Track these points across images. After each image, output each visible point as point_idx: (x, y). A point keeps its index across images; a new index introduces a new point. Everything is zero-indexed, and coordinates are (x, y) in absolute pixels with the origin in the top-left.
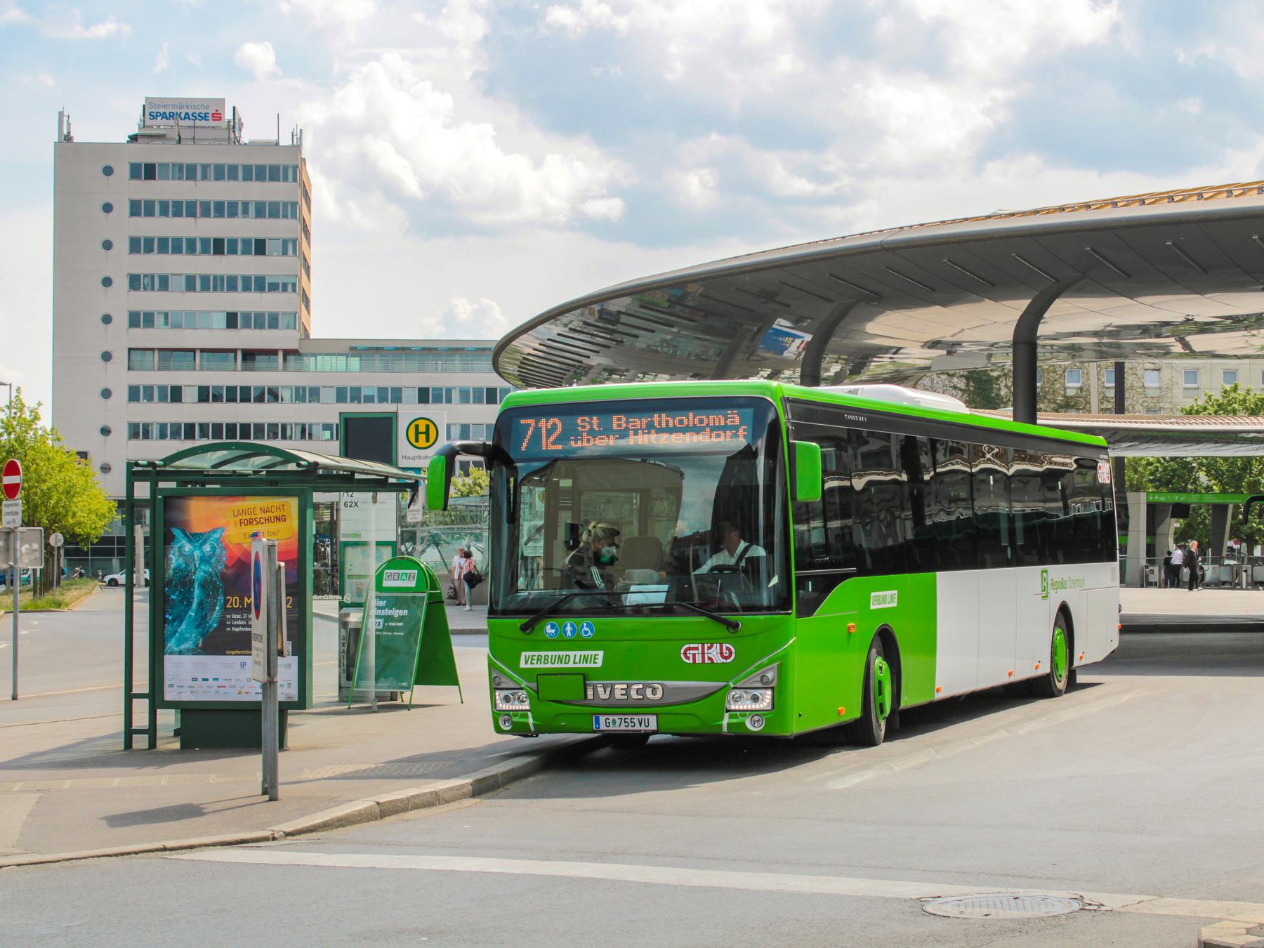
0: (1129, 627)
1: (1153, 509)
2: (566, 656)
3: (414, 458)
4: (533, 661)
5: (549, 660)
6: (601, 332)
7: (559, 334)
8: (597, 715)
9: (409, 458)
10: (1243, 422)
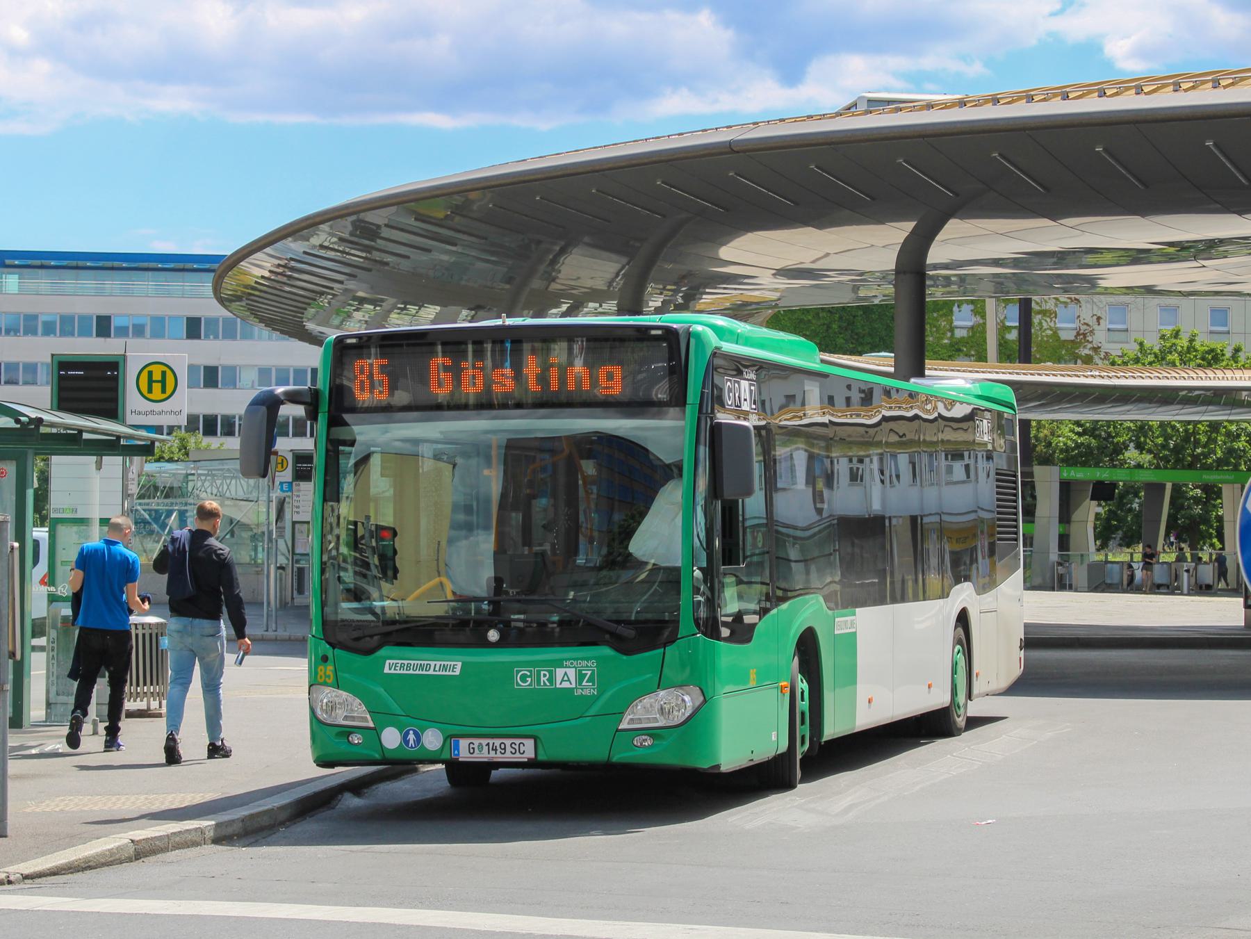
0: (1035, 640)
1: (1067, 491)
3: (146, 414)
4: (397, 668)
5: (412, 667)
6: (354, 249)
7: (305, 253)
9: (140, 413)
10: (1186, 375)
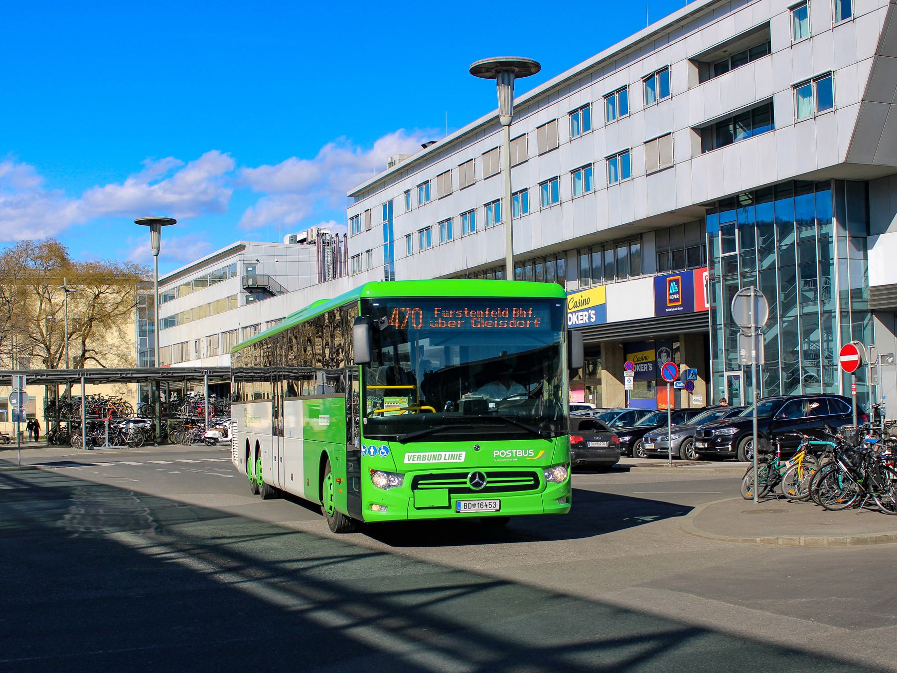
2: (439, 455)
4: (414, 459)
5: (427, 458)
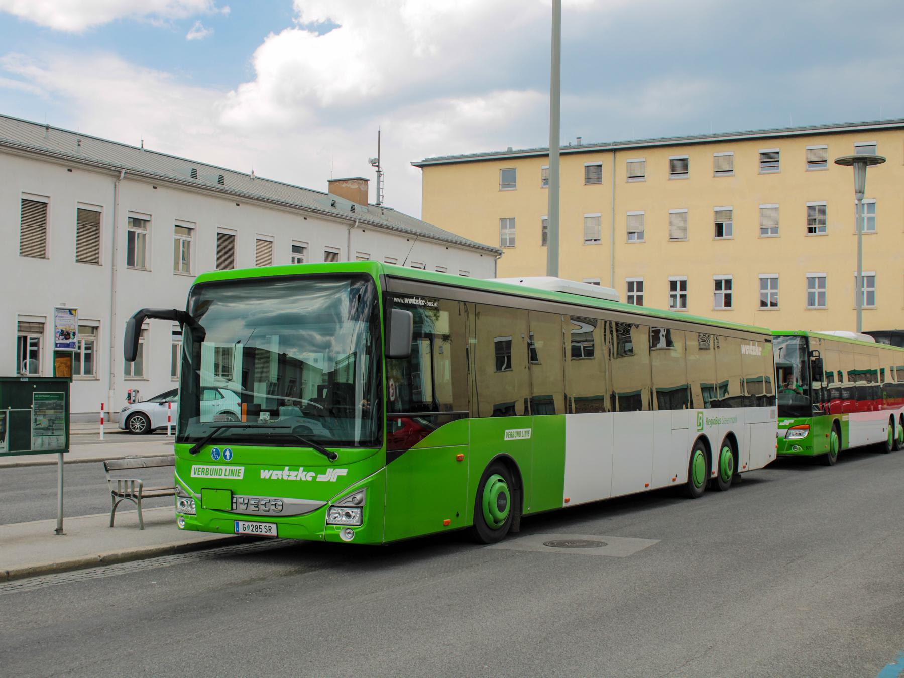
2: (220, 469)
5: (209, 472)
8: (237, 521)
